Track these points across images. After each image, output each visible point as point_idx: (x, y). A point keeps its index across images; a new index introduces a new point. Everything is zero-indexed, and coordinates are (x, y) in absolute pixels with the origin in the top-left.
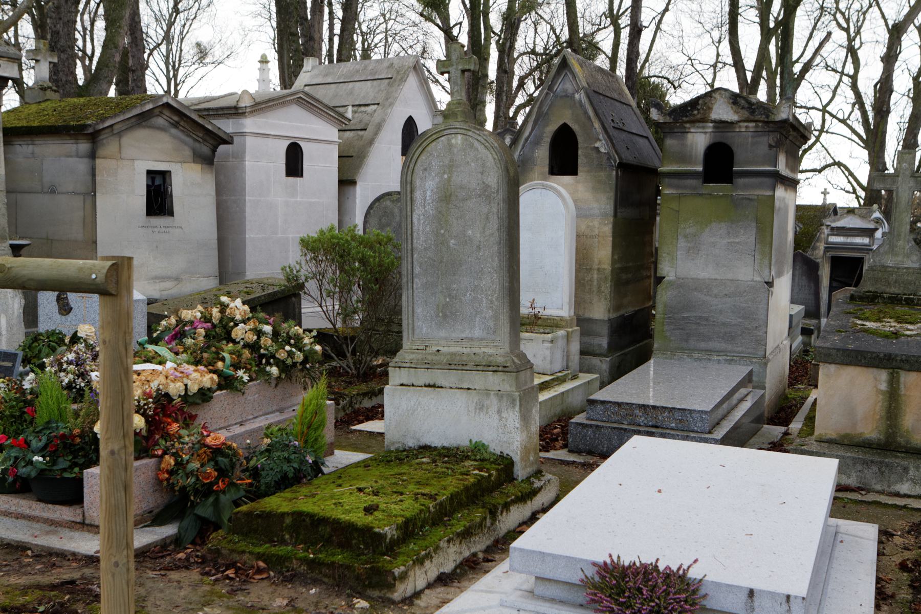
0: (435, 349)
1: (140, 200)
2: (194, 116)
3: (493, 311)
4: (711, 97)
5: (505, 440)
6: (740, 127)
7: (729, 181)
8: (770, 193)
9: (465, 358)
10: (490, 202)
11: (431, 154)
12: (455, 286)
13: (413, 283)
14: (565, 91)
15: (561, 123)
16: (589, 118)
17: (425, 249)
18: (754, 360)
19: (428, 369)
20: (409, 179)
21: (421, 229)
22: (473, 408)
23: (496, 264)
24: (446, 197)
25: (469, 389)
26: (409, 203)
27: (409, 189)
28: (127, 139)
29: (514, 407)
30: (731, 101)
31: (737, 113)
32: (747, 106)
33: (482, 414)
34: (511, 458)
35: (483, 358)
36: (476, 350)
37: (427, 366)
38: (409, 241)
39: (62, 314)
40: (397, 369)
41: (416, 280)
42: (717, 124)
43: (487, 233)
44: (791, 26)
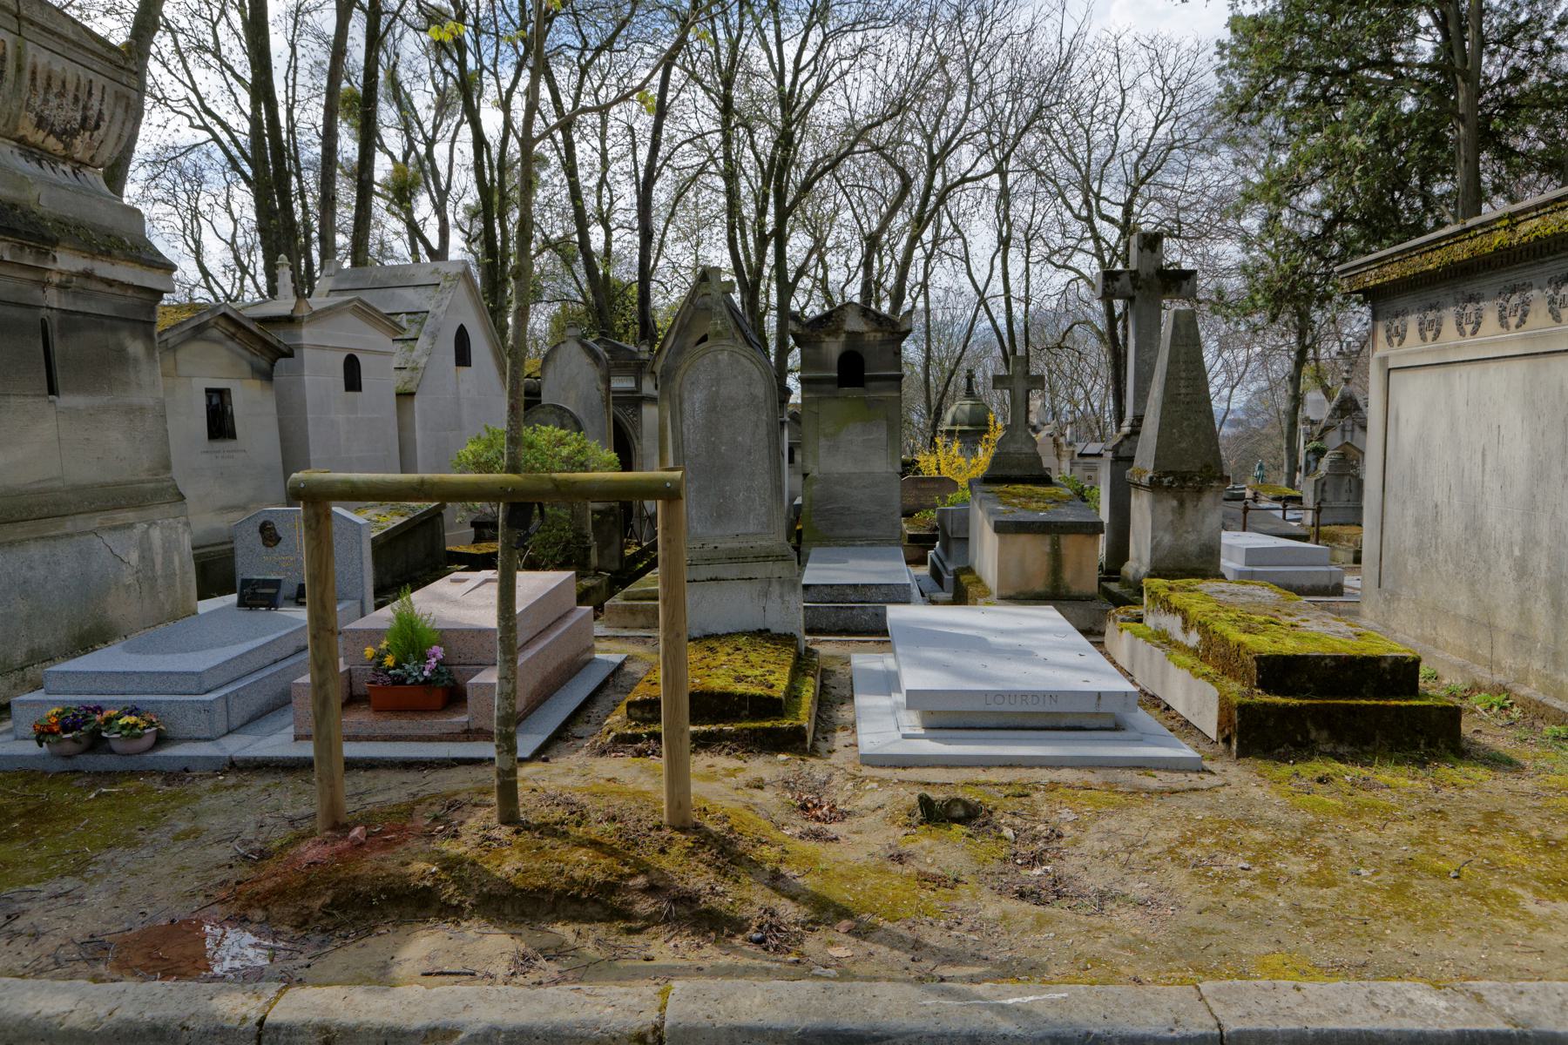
1: (199, 422)
2: (254, 327)
7: (861, 385)
8: (897, 394)
23: (766, 466)
24: (712, 408)
28: (182, 354)
36: (753, 544)
39: (268, 546)
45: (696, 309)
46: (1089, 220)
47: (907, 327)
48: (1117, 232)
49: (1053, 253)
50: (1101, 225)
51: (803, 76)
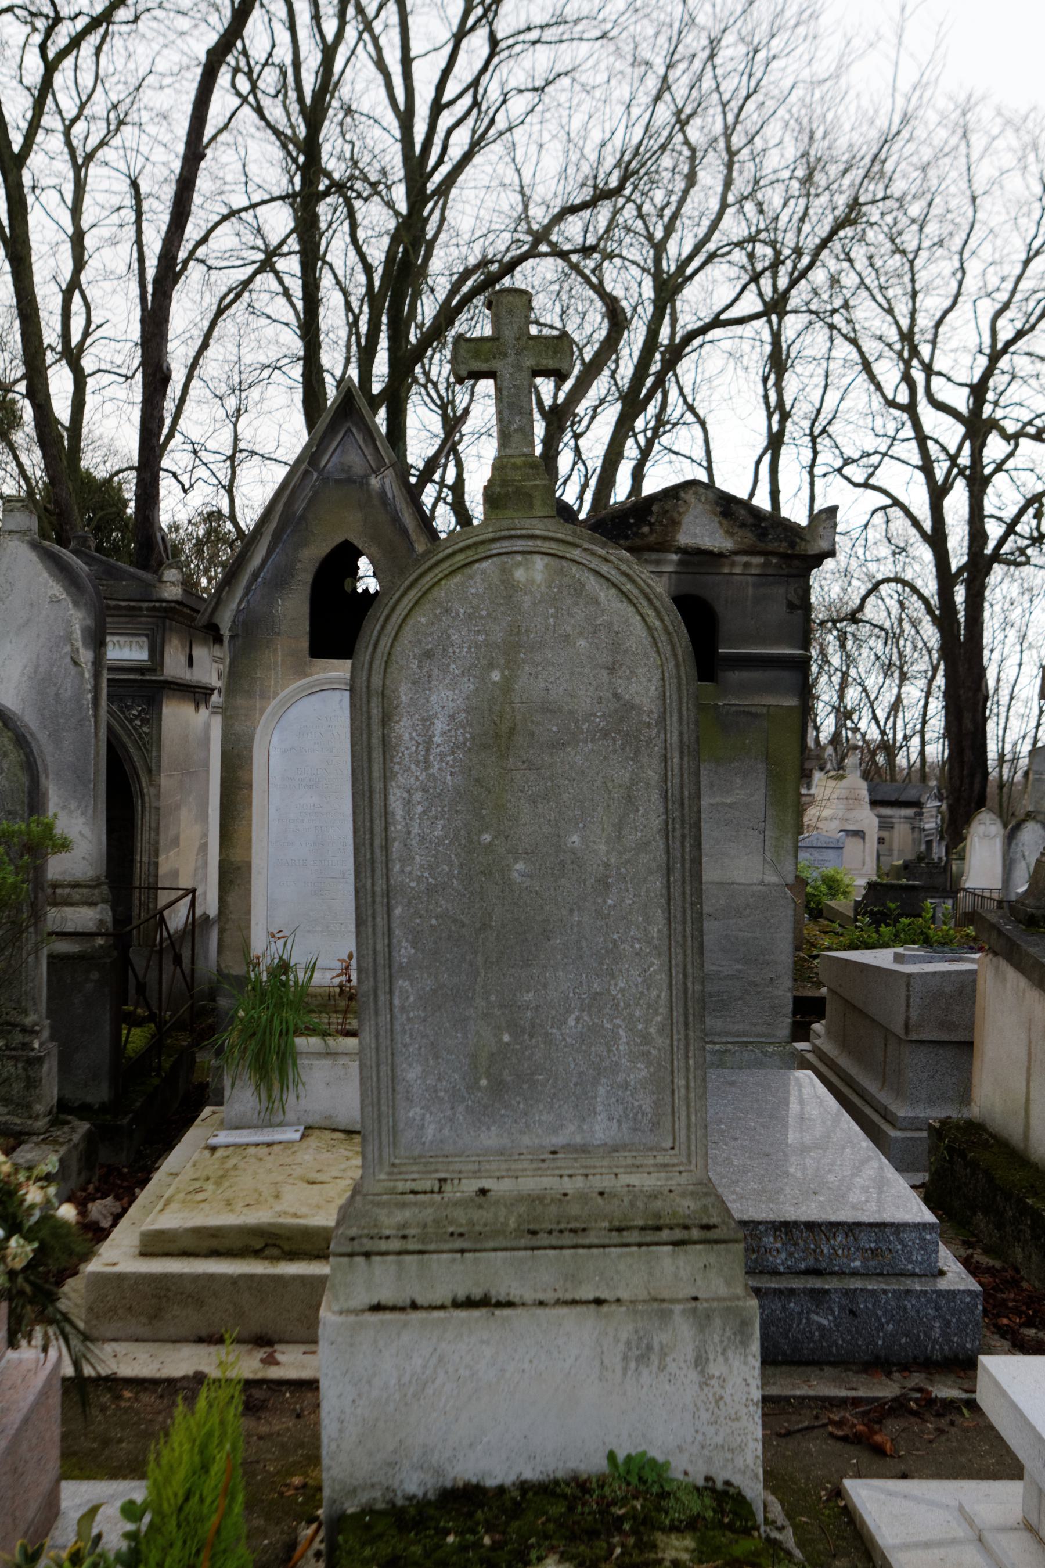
0: (471, 1186)
3: (649, 1064)
4: (678, 499)
5: (719, 1440)
6: (733, 564)
9: (575, 1210)
10: (637, 752)
11: (447, 611)
12: (529, 997)
13: (391, 992)
14: (347, 469)
15: (339, 539)
16: (404, 531)
17: (430, 891)
18: (770, 1049)
19: (462, 1251)
20: (377, 681)
21: (416, 830)
22: (619, 1358)
23: (657, 928)
25: (599, 1302)
26: (377, 754)
27: (376, 712)
29: (745, 1344)
30: (719, 509)
31: (732, 535)
32: (750, 520)
33: (645, 1372)
34: (739, 1493)
35: (632, 1204)
36: (605, 1182)
37: (459, 1244)
38: (379, 867)
40: (360, 1260)
41: (402, 983)
42: (686, 557)
43: (631, 839)
44: (403, 395)
45: (325, 480)
46: (911, 409)
47: (824, 545)
48: (961, 430)
49: (848, 461)
50: (931, 419)
51: (446, 120)
